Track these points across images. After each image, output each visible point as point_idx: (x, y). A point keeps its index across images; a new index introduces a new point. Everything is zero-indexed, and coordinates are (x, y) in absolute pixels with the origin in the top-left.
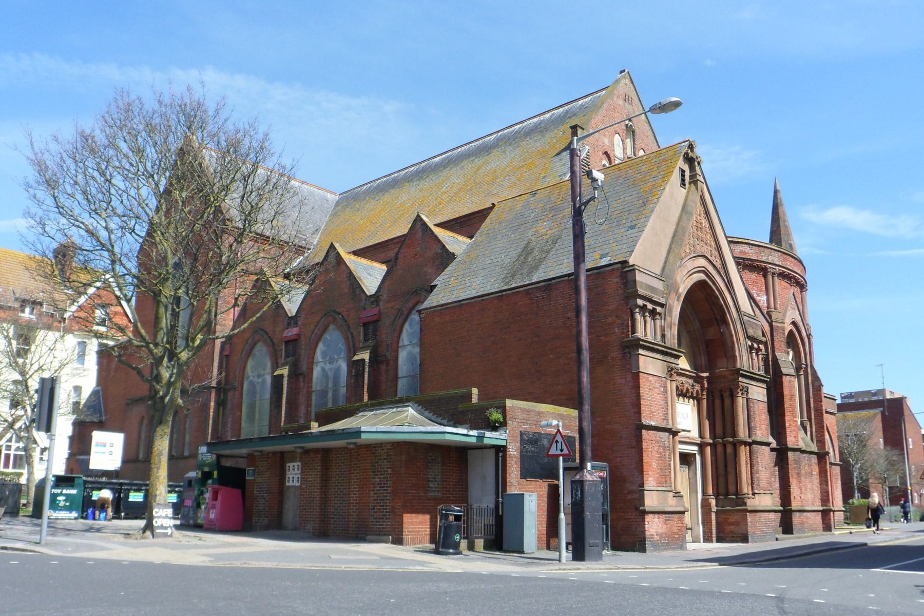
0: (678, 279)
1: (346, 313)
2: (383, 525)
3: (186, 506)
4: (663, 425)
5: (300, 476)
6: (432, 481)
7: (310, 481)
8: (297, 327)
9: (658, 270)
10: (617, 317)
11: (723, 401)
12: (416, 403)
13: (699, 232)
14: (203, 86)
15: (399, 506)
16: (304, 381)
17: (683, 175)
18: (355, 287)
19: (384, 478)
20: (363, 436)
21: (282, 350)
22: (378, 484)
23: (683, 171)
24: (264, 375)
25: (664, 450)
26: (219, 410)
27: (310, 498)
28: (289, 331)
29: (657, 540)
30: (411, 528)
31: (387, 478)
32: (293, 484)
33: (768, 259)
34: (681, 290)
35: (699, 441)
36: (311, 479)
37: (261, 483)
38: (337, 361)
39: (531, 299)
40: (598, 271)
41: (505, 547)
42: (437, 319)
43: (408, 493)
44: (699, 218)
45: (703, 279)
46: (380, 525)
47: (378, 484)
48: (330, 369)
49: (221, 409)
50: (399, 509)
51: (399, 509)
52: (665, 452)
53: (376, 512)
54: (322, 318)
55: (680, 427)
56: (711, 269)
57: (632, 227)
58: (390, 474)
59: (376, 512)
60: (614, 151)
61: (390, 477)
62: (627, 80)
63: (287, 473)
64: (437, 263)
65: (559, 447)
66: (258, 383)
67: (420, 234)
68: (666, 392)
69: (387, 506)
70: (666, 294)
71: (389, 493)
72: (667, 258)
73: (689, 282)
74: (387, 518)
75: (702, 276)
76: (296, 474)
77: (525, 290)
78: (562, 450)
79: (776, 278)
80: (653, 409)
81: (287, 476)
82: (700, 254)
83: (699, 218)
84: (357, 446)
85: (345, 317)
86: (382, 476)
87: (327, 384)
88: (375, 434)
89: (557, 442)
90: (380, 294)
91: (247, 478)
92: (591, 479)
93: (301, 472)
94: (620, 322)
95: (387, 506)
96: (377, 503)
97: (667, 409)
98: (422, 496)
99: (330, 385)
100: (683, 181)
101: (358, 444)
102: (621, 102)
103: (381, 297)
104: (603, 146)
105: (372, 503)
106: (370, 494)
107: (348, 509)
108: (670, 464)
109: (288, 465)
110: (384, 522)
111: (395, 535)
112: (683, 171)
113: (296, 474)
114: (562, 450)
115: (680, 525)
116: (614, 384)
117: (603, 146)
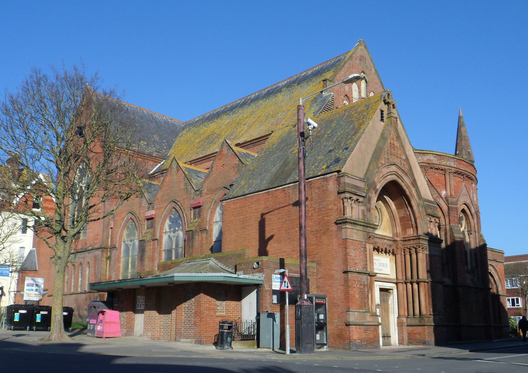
0: (376, 180)
1: (183, 201)
2: (189, 332)
3: (92, 324)
4: (364, 271)
5: (144, 303)
6: (219, 306)
7: (150, 306)
8: (153, 210)
9: (362, 176)
10: (334, 205)
11: (411, 255)
12: (214, 258)
13: (392, 150)
14: (83, 67)
15: (198, 321)
16: (158, 244)
17: (382, 114)
18: (188, 185)
19: (190, 304)
20: (378, 275)
21: (144, 224)
22: (187, 308)
23: (382, 111)
24: (134, 240)
25: (364, 286)
26: (107, 262)
27: (150, 316)
28: (149, 213)
29: (359, 343)
30: (206, 334)
31: (192, 304)
32: (141, 308)
33: (446, 164)
34: (378, 187)
35: (395, 281)
36: (150, 305)
37: (122, 308)
38: (177, 231)
39: (286, 194)
40: (324, 176)
41: (260, 347)
42: (232, 206)
43: (204, 313)
44: (392, 141)
45: (394, 179)
46: (188, 332)
47: (187, 308)
48: (174, 237)
49: (108, 261)
50: (198, 323)
51: (198, 323)
52: (365, 288)
53: (186, 325)
54: (168, 204)
55: (375, 271)
56: (400, 173)
57: (346, 149)
58: (194, 302)
59: (186, 325)
60: (352, 94)
61: (194, 304)
62: (362, 47)
63: (137, 301)
64: (235, 170)
65: (286, 285)
66: (130, 245)
67: (175, 170)
68: (366, 251)
69: (192, 321)
70: (366, 190)
71: (193, 313)
72: (368, 167)
73: (383, 182)
74: (192, 328)
75: (394, 177)
76: (142, 302)
77: (282, 188)
78: (288, 287)
79: (452, 175)
80: (357, 261)
81: (138, 303)
82: (393, 163)
83: (392, 141)
84: (175, 285)
85: (182, 203)
86: (189, 303)
87: (172, 246)
88: (407, 271)
89: (285, 282)
90: (203, 189)
91: (114, 305)
92: (307, 304)
93: (145, 301)
94: (336, 208)
95: (192, 321)
96: (187, 319)
97: (366, 261)
98: (213, 315)
99: (174, 247)
100: (382, 117)
101: (175, 284)
102: (358, 62)
103: (203, 191)
104: (344, 92)
105: (184, 319)
106: (182, 314)
107: (171, 323)
108: (368, 296)
109: (137, 297)
110: (190, 330)
111: (196, 338)
112: (382, 111)
113: (142, 302)
114: (288, 287)
115: (375, 333)
116: (332, 246)
117: (344, 92)
